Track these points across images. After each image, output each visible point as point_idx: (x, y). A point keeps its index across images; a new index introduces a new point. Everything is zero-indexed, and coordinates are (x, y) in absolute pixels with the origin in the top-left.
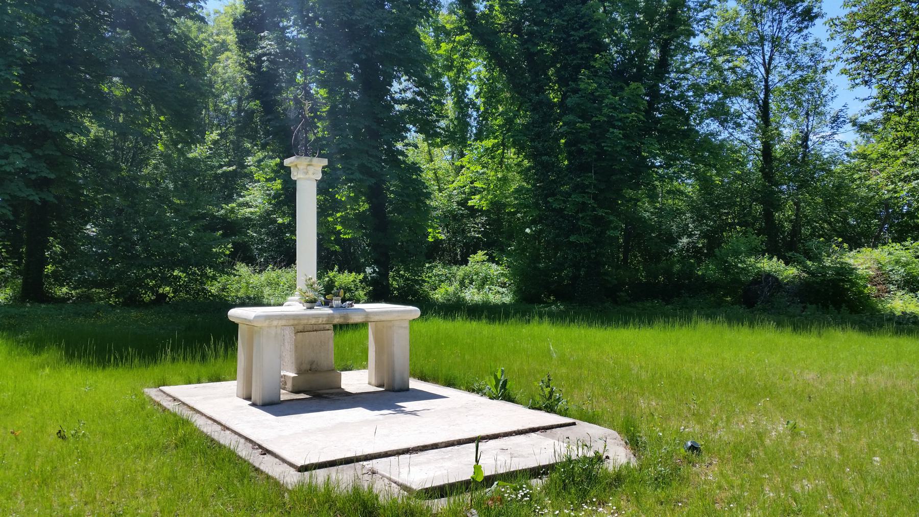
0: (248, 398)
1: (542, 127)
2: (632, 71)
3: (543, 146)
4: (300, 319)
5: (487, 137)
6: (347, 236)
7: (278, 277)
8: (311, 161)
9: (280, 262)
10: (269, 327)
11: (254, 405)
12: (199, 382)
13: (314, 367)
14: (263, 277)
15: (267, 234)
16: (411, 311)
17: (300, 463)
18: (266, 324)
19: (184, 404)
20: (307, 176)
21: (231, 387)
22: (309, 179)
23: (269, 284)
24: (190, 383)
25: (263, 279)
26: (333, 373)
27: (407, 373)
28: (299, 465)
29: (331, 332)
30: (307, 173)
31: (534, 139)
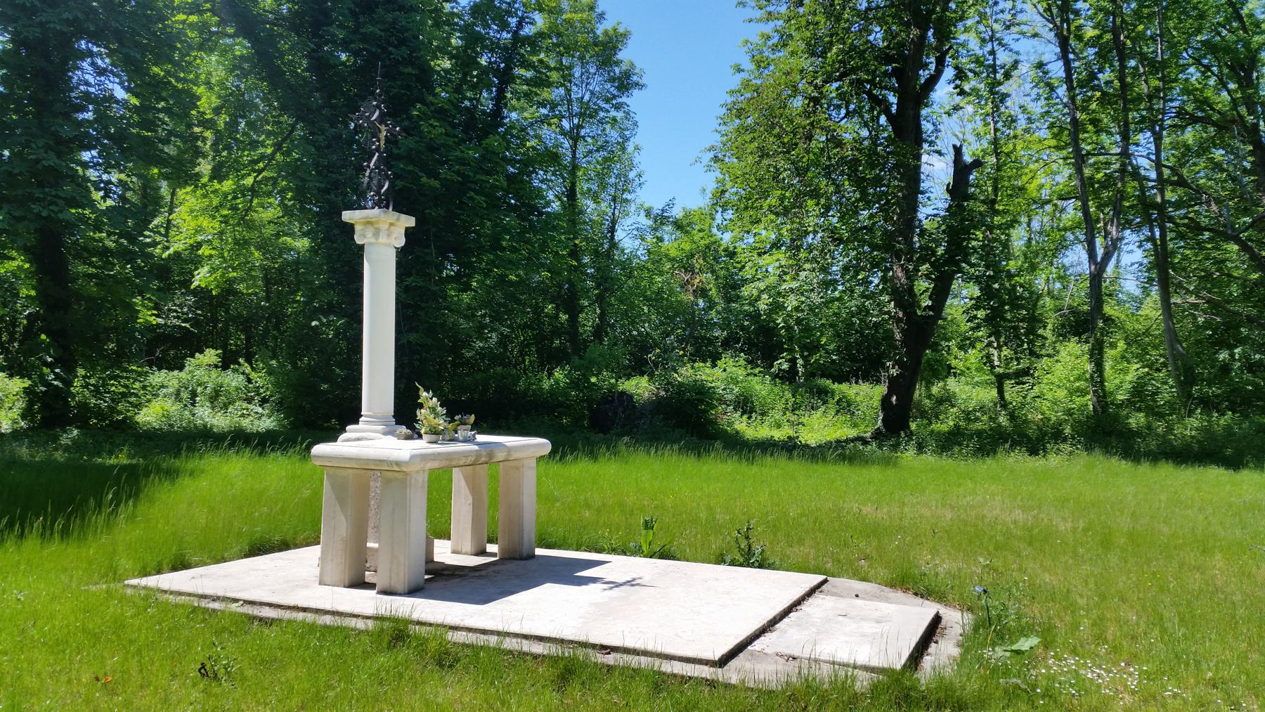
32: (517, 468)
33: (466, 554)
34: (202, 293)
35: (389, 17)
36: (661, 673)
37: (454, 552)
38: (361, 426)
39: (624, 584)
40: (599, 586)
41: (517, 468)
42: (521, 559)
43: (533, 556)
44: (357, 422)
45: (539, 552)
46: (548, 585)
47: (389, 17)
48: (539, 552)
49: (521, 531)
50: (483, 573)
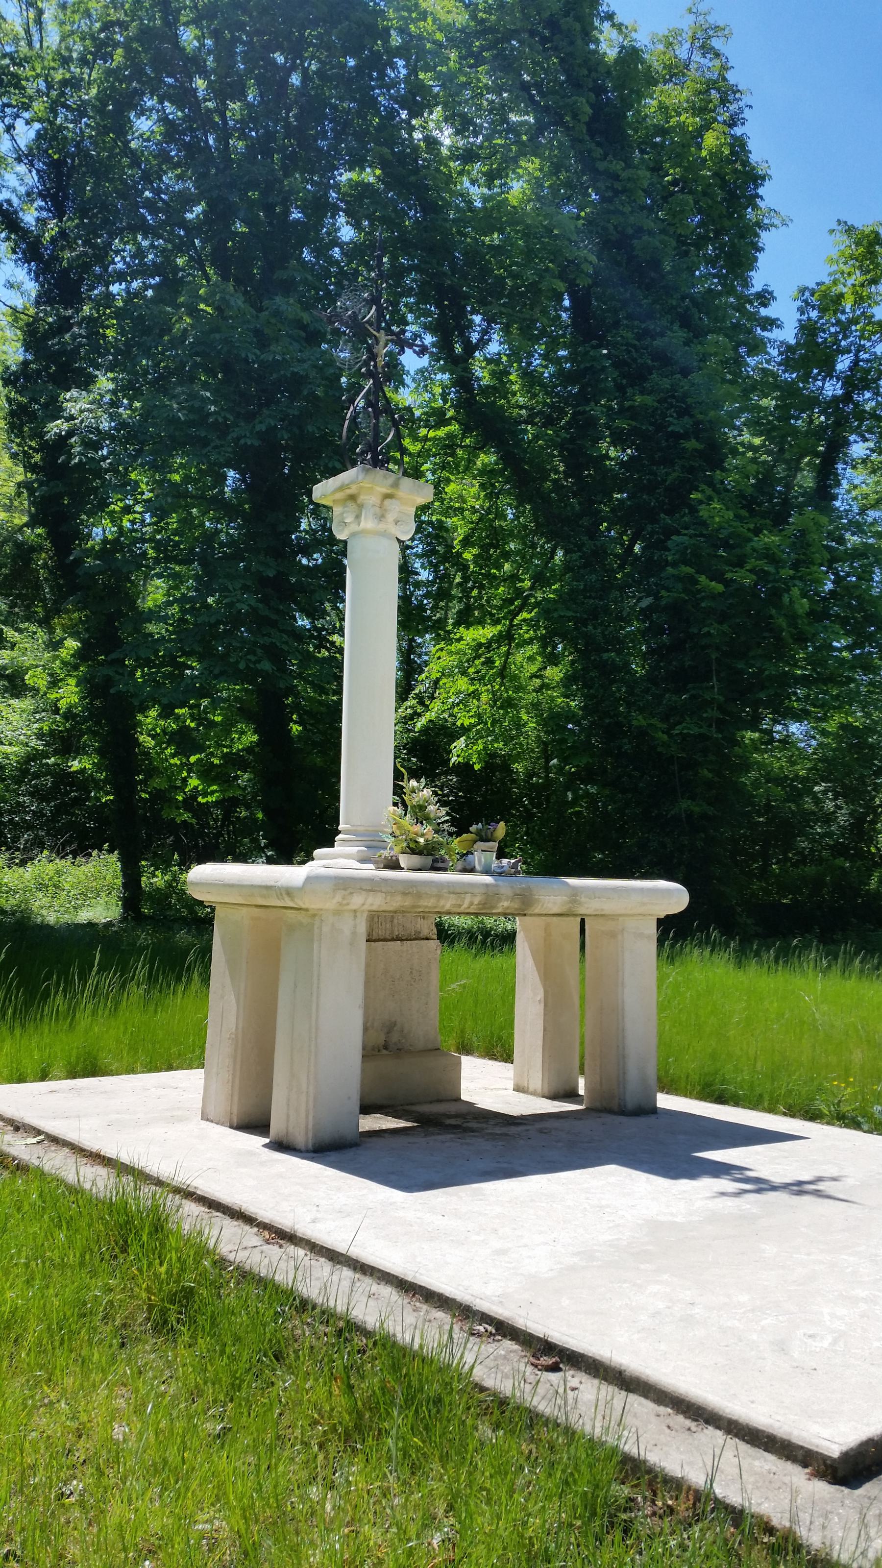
0: (256, 1124)
1: (601, 599)
2: (765, 503)
3: (603, 633)
4: (419, 896)
5: (481, 622)
6: (209, 799)
7: (59, 873)
8: (396, 485)
9: (63, 846)
10: (337, 913)
11: (281, 1146)
12: (44, 1076)
13: (395, 1037)
14: (29, 873)
15: (31, 794)
16: (668, 891)
17: (836, 1438)
18: (331, 904)
19: (55, 1140)
20: (382, 527)
21: (187, 1085)
22: (384, 534)
23: (41, 887)
24: (21, 1080)
25: (27, 875)
26: (439, 1059)
27: (652, 1073)
28: (834, 1451)
29: (435, 944)
30: (381, 517)
31: (578, 625)
32: (613, 935)
33: (534, 1094)
34: (464, 769)
35: (666, 383)
36: (633, 1468)
37: (518, 1089)
38: (338, 848)
39: (785, 1187)
40: (725, 1184)
41: (613, 935)
42: (623, 1112)
43: (653, 1110)
44: (331, 844)
45: (665, 1101)
46: (612, 1167)
47: (666, 383)
48: (665, 1101)
49: (622, 1058)
50: (513, 1130)
